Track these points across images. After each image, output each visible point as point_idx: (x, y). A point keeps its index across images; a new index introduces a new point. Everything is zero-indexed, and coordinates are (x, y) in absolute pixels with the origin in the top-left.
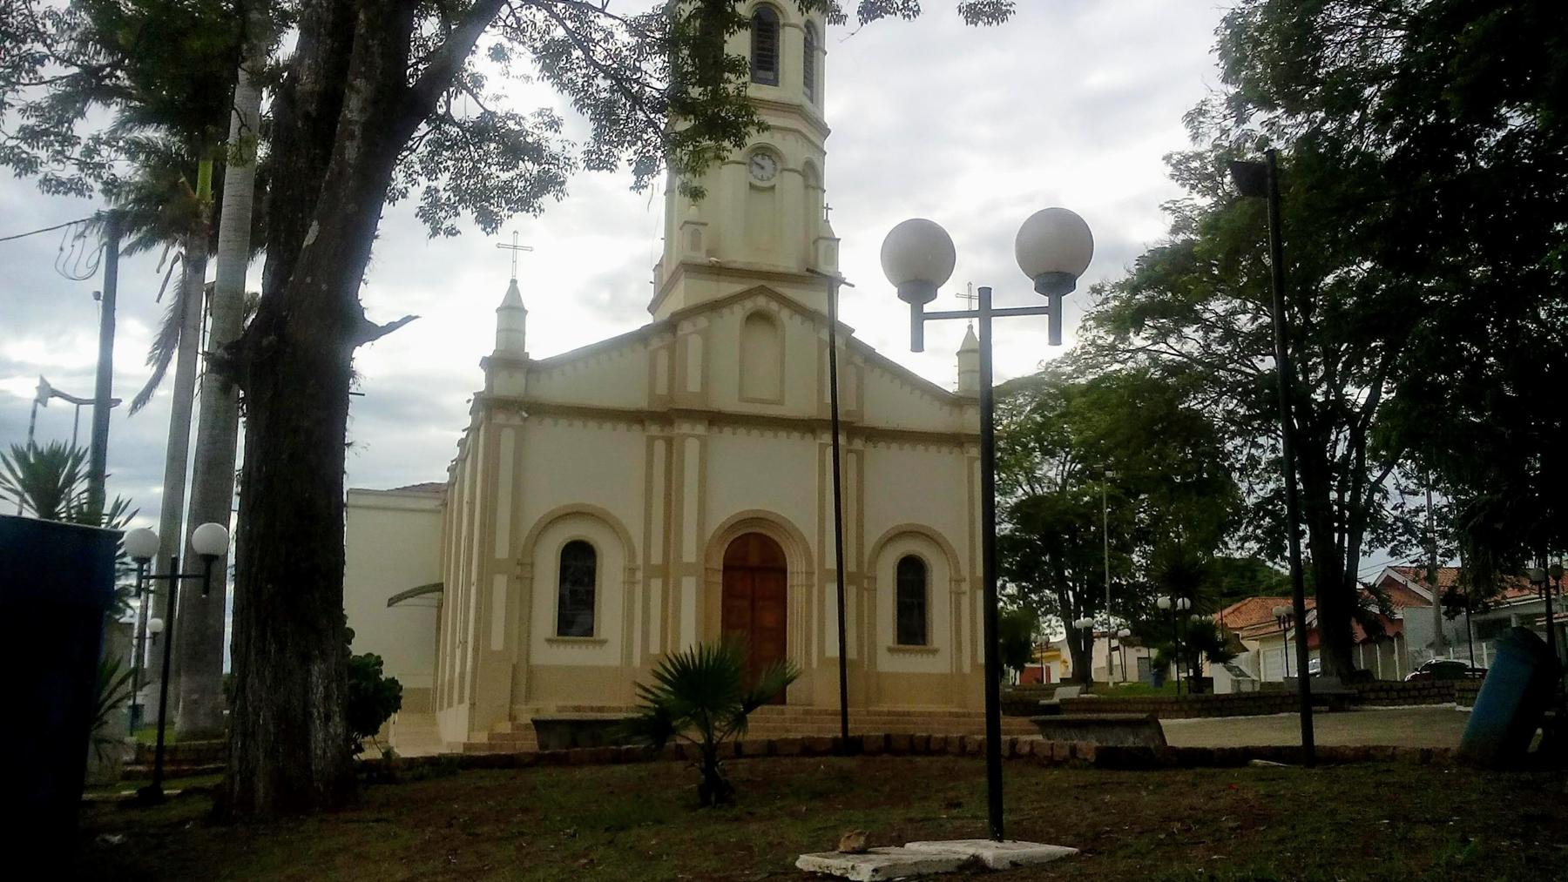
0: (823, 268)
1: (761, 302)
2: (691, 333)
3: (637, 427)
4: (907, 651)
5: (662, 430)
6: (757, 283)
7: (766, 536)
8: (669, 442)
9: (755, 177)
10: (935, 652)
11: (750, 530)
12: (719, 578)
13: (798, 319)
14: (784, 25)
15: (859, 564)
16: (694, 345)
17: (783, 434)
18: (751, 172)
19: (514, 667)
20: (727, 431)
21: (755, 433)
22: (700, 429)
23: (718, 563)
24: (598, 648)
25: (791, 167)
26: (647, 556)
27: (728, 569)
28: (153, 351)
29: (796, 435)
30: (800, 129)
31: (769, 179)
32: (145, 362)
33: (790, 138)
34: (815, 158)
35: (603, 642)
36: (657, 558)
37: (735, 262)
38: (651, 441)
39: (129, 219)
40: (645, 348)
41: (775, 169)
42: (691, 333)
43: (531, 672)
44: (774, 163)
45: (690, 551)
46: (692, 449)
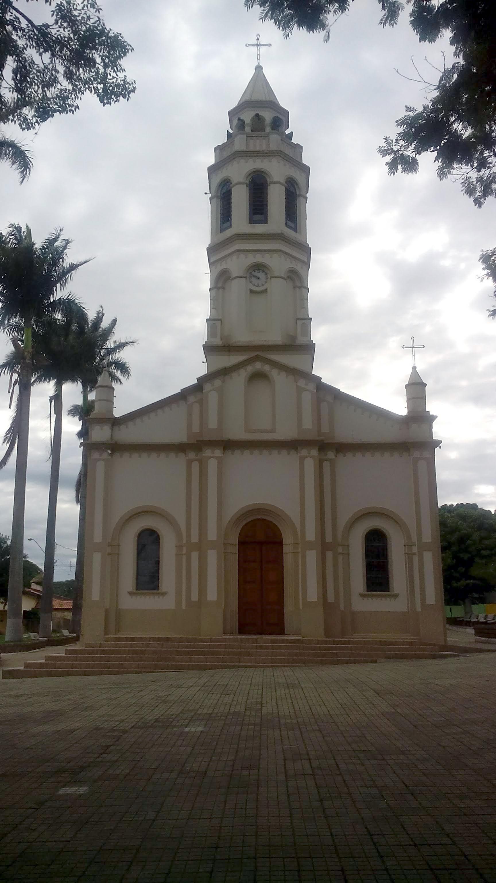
0: (301, 340)
1: (258, 366)
2: (211, 391)
3: (181, 455)
4: (373, 596)
5: (197, 455)
6: (253, 354)
7: (269, 521)
8: (200, 462)
9: (254, 285)
10: (396, 596)
11: (255, 518)
12: (235, 549)
13: (283, 374)
14: (271, 183)
15: (335, 535)
16: (213, 399)
17: (275, 452)
18: (251, 282)
19: (107, 611)
20: (237, 452)
21: (256, 452)
22: (218, 452)
23: (234, 539)
24: (161, 597)
25: (276, 274)
26: (189, 536)
27: (242, 544)
28: (6, 435)
29: (284, 452)
30: (281, 249)
31: (263, 285)
32: (2, 441)
33: (276, 256)
34: (298, 267)
35: (164, 594)
36: (195, 539)
37: (240, 341)
38: (189, 463)
39: (13, 363)
40: (186, 403)
41: (267, 278)
42: (211, 391)
43: (119, 613)
44: (266, 274)
45: (212, 535)
46: (212, 465)
